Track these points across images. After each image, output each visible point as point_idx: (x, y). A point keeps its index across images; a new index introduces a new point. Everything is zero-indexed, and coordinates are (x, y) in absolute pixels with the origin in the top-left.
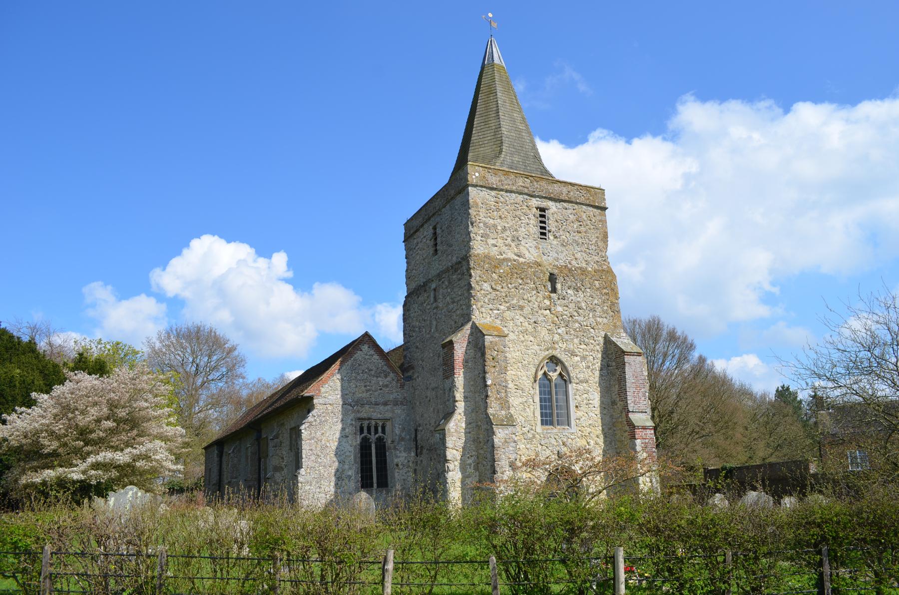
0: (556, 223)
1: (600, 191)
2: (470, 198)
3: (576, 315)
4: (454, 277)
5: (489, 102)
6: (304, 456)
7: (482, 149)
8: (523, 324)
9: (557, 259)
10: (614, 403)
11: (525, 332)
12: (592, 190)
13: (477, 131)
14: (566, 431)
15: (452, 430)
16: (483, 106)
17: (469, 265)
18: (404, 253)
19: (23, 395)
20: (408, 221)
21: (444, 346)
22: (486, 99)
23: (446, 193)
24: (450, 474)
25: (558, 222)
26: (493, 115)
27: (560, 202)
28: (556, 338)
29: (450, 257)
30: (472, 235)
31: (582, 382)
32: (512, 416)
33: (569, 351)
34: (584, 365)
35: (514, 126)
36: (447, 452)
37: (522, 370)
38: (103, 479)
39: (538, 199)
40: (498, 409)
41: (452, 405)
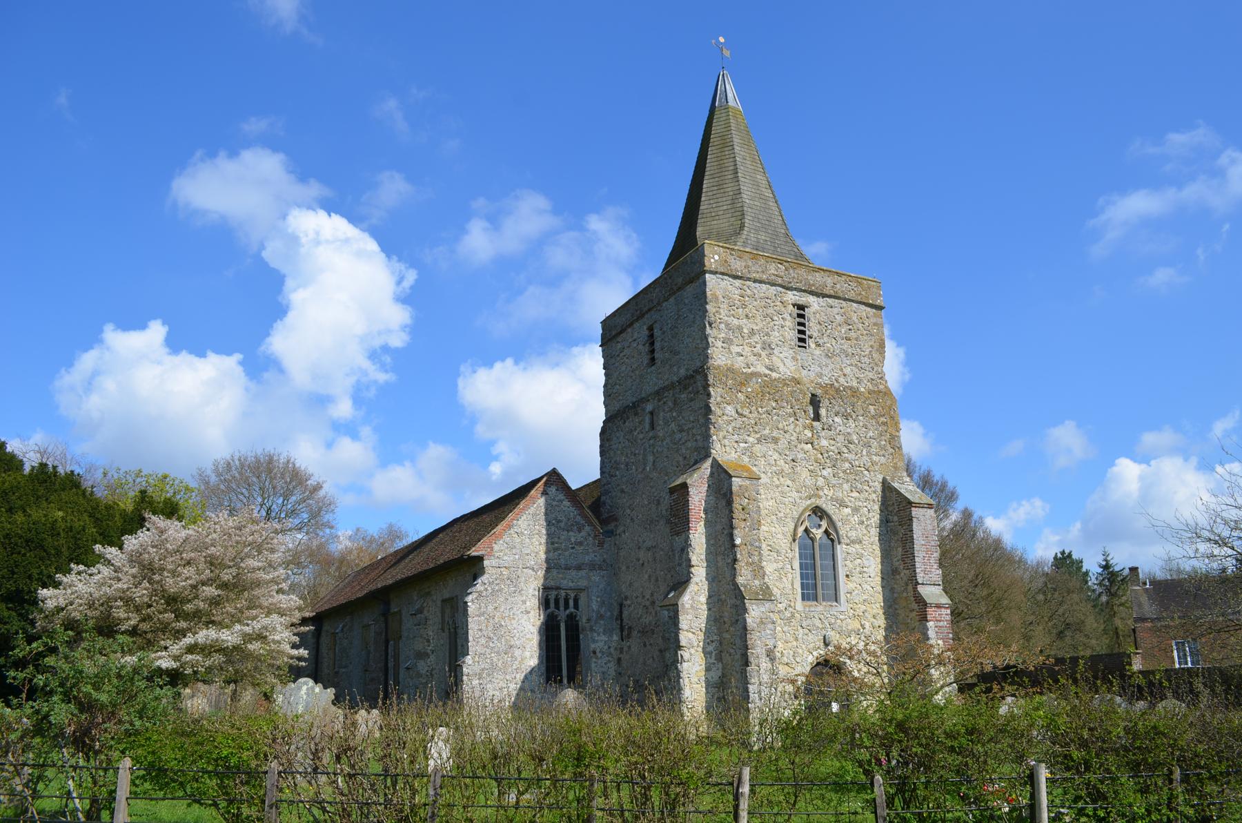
0: (818, 326)
1: (874, 283)
2: (707, 290)
3: (846, 451)
4: (683, 396)
5: (723, 158)
6: (470, 638)
7: (715, 222)
8: (778, 462)
9: (820, 375)
10: (895, 572)
11: (780, 473)
12: (865, 282)
13: (708, 198)
14: (834, 608)
15: (687, 606)
16: (716, 164)
17: (706, 379)
18: (602, 361)
19: (69, 548)
20: (608, 318)
21: (672, 491)
22: (719, 154)
23: (670, 281)
24: (685, 665)
25: (821, 325)
26: (729, 177)
27: (823, 297)
28: (821, 482)
29: (675, 369)
30: (710, 340)
31: (853, 542)
32: (768, 587)
33: (837, 500)
34: (856, 519)
35: (758, 192)
36: (680, 635)
37: (776, 526)
38: (202, 667)
39: (795, 292)
40: (749, 577)
41: (685, 572)
